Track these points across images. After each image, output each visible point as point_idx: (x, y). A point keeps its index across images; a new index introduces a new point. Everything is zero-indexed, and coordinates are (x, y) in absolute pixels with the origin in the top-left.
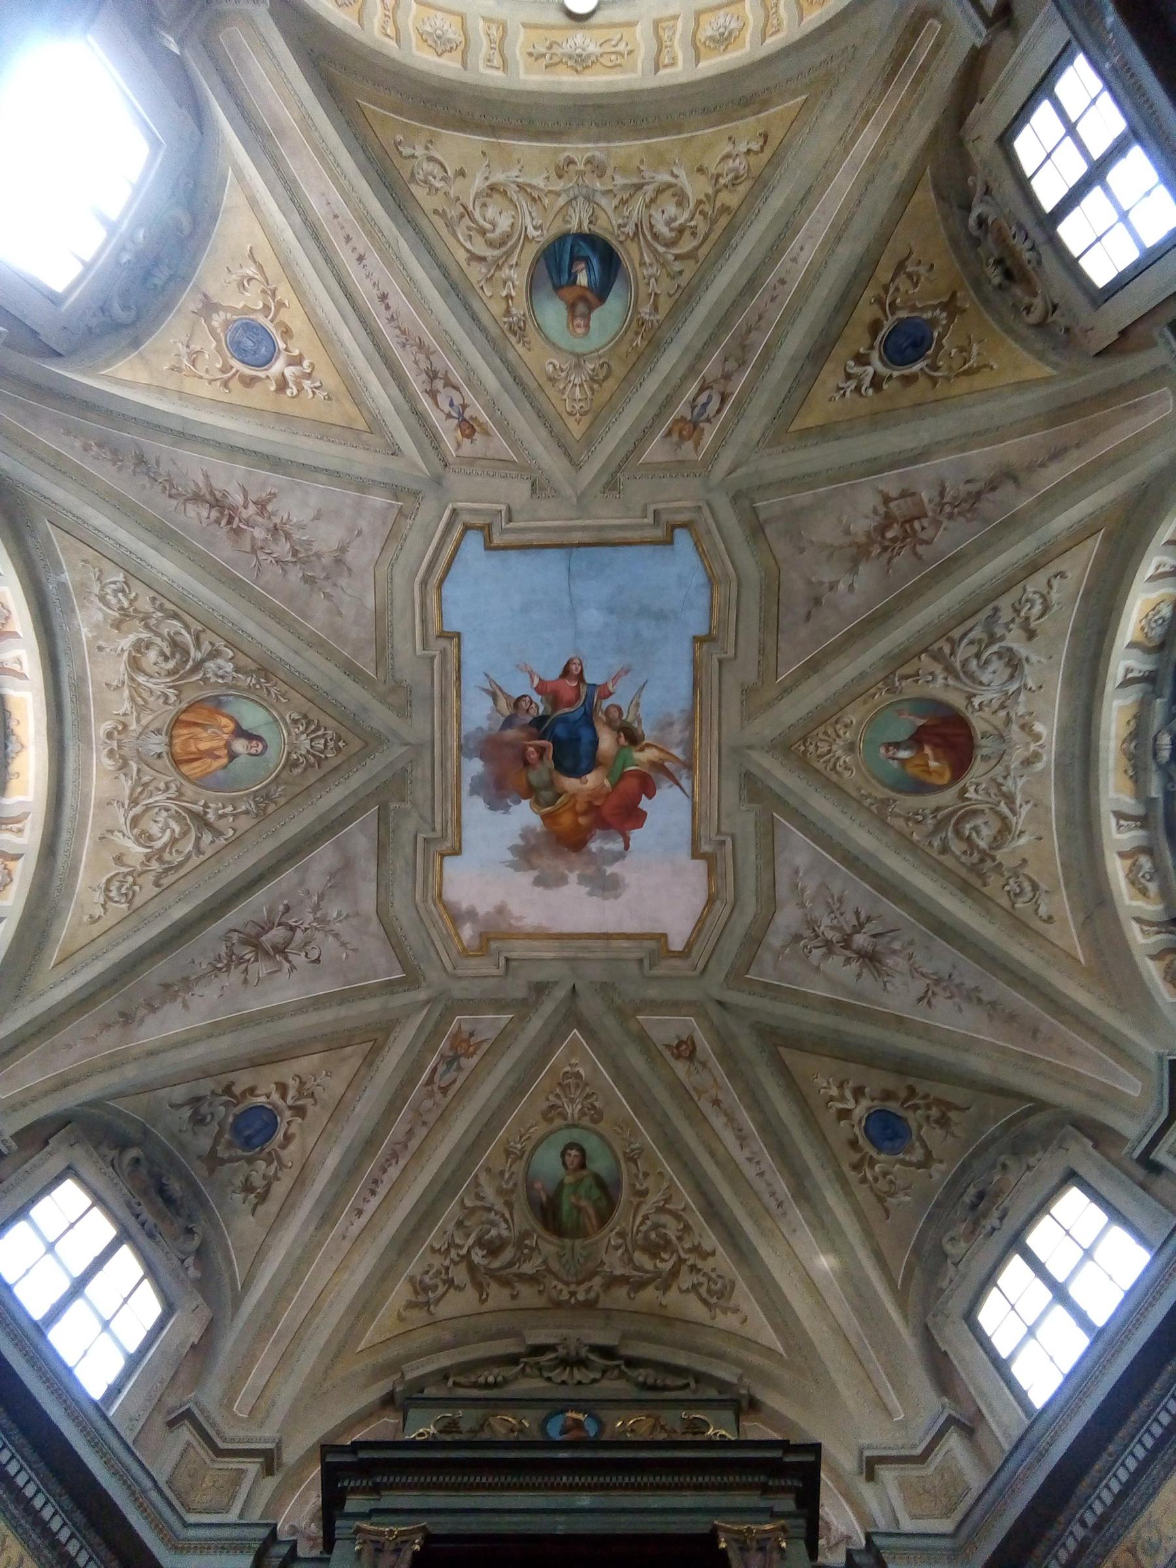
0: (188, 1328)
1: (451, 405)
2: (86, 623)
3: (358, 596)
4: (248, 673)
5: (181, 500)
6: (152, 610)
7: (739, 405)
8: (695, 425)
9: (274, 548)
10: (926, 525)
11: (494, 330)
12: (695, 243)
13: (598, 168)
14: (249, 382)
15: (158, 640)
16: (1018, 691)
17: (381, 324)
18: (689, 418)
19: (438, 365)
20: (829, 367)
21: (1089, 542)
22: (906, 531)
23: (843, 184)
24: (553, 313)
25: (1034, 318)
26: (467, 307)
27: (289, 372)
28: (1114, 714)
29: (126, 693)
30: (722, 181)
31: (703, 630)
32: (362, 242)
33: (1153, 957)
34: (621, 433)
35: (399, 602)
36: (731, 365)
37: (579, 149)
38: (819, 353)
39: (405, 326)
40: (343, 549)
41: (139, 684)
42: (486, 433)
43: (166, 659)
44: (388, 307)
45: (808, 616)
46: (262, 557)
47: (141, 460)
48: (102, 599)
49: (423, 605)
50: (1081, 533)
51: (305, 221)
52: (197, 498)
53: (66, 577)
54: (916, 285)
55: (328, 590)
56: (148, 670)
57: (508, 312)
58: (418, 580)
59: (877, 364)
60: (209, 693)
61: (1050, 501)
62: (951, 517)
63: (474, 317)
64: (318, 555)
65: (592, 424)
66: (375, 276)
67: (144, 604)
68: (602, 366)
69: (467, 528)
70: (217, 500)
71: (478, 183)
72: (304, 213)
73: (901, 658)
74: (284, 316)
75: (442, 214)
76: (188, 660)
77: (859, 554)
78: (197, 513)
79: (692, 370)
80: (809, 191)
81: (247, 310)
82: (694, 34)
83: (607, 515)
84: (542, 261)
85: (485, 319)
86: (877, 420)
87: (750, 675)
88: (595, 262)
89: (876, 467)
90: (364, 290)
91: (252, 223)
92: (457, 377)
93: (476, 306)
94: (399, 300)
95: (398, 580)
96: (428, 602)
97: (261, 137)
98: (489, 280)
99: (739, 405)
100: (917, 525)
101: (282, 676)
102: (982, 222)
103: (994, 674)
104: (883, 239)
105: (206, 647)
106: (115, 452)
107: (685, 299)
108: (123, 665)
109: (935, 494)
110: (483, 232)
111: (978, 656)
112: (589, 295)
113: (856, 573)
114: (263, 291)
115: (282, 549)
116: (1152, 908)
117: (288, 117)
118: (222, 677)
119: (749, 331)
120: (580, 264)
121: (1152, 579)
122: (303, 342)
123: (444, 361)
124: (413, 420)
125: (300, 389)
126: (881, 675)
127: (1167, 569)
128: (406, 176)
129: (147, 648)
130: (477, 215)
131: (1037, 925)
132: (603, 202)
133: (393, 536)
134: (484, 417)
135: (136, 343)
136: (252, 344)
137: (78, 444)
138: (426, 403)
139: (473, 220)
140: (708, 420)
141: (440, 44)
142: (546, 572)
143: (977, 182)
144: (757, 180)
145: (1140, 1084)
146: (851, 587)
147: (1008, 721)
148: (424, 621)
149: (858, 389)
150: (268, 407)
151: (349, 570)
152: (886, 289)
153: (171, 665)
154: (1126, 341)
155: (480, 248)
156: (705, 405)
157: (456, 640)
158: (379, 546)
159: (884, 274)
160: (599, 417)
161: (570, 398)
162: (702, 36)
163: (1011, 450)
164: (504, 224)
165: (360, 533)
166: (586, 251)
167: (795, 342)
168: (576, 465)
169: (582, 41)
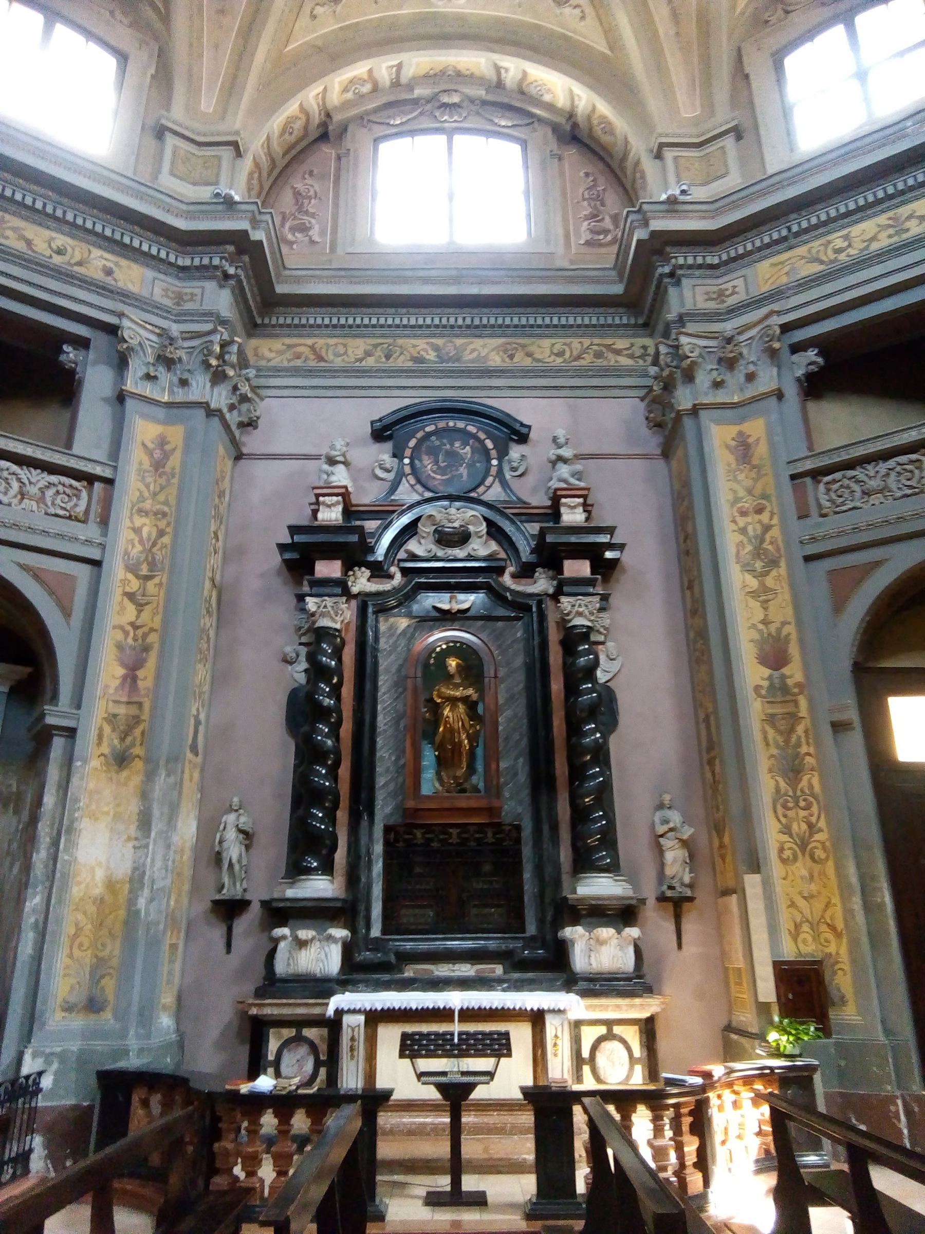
21: (604, 43)
28: (474, 59)
33: (301, 105)
50: (610, 34)
116: (335, 98)
121: (571, 92)
127: (576, 102)
131: (307, 9)
145: (211, 110)
154: (740, 76)
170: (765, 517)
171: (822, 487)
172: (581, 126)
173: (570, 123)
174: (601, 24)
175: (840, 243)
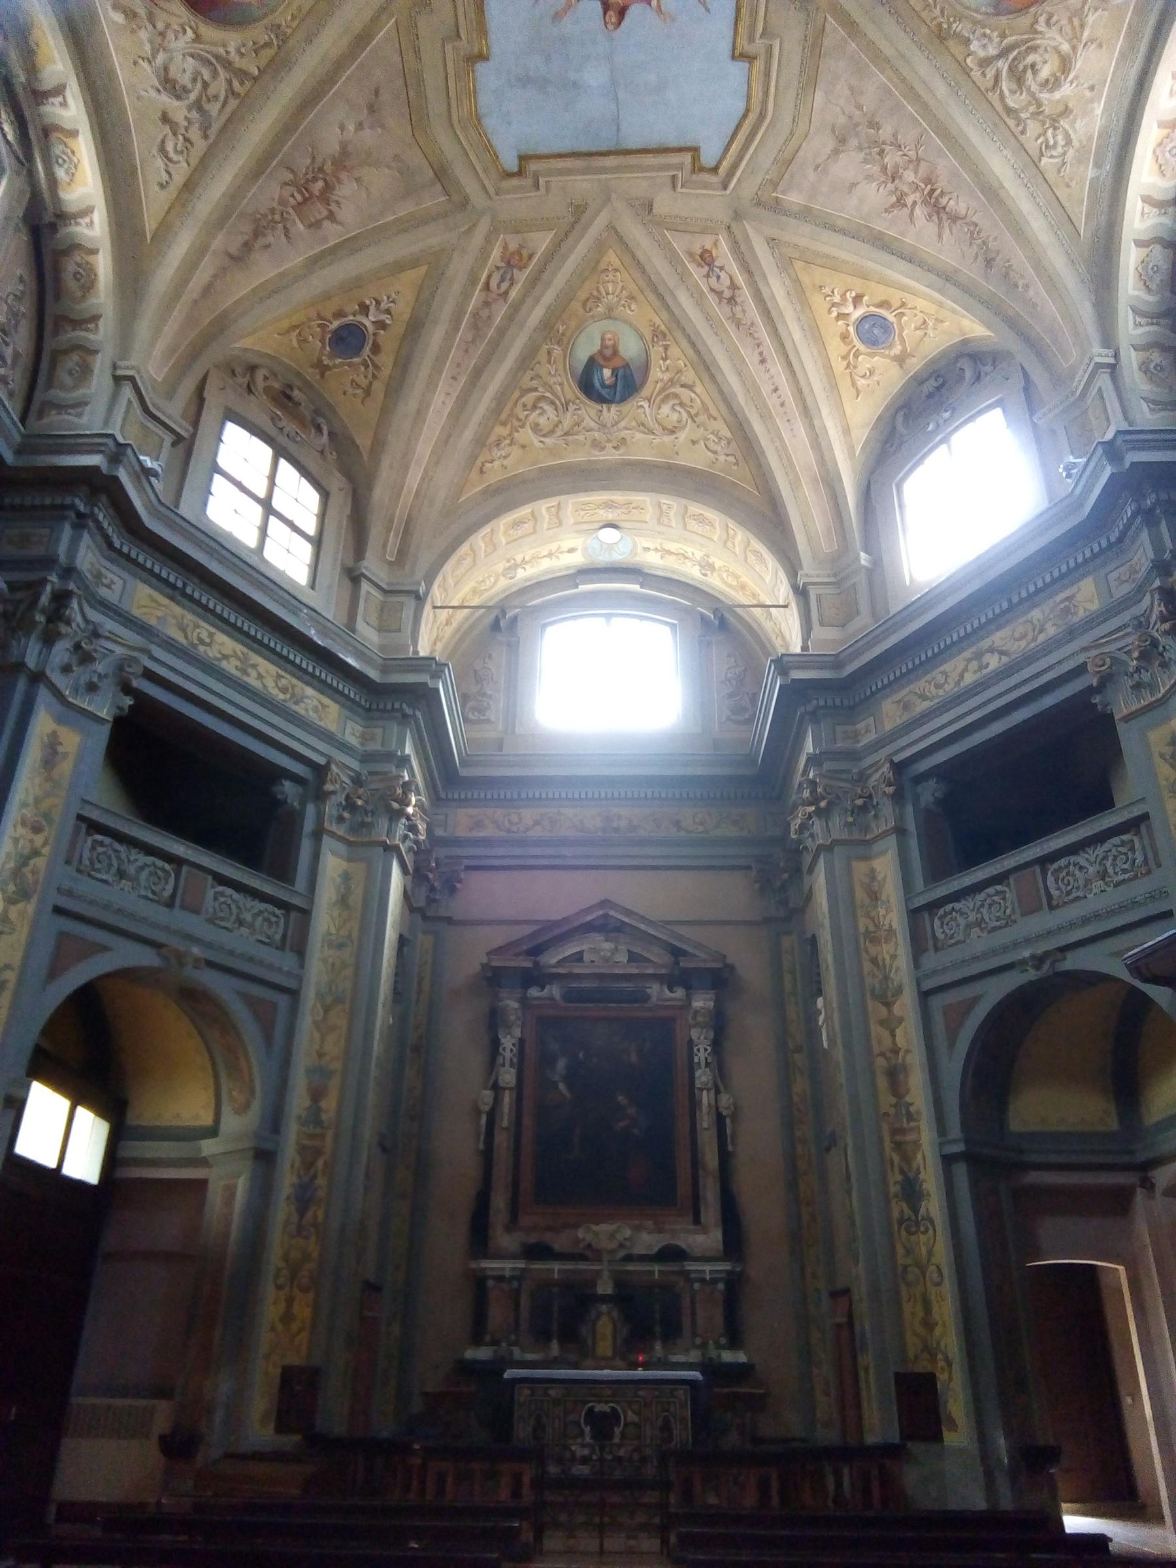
0: (341, 500)
1: (718, 277)
2: (1093, 120)
3: (830, 104)
4: (957, 35)
5: (968, 220)
6: (1029, 121)
7: (473, 281)
8: (508, 263)
9: (897, 159)
10: (291, 199)
11: (678, 334)
12: (524, 399)
13: (596, 445)
14: (884, 304)
15: (1034, 88)
16: (154, 56)
17: (767, 340)
18: (515, 271)
19: (727, 309)
20: (406, 317)
21: (154, 226)
22: (307, 190)
23: (424, 449)
24: (630, 348)
25: (260, 374)
26: (698, 352)
27: (849, 309)
29: (1086, 34)
30: (508, 441)
31: (480, 67)
32: (772, 402)
34: (572, 257)
35: (791, 94)
36: (484, 313)
37: (611, 455)
38: (415, 328)
39: (749, 339)
40: (836, 152)
41: (1070, 41)
42: (691, 254)
43: (1033, 66)
44: (761, 354)
45: (377, 93)
46: (912, 153)
47: (989, 263)
48: (1069, 142)
49: (766, 93)
50: (165, 230)
51: (811, 420)
52: (955, 218)
53: (1091, 173)
54: (353, 381)
55: (858, 112)
56: (1056, 57)
57: (666, 348)
58: (768, 120)
59: (368, 322)
60: (1004, 20)
61: (199, 252)
62: (273, 211)
63: (693, 345)
64: (860, 148)
65: (598, 262)
66: (767, 376)
67: (1033, 128)
68: (590, 310)
69: (715, 170)
70: (938, 214)
71: (682, 436)
72: (811, 426)
73: (277, 66)
74: (844, 349)
75: (710, 416)
76: (1015, 59)
77: (343, 160)
78: (959, 204)
79: (516, 308)
80: (446, 442)
81: (872, 355)
82: (535, 524)
83: (583, 185)
84: (638, 382)
85: (684, 343)
86: (358, 282)
87: (424, 25)
88: (597, 384)
89: (349, 246)
90: (777, 367)
91: (849, 420)
92: (711, 298)
93: (690, 352)
94: (750, 358)
95: (788, 119)
96: (761, 93)
97: (830, 483)
98: (679, 371)
99: (473, 281)
100: (299, 197)
101: (924, 30)
102: (319, 429)
103: (184, 69)
104: (386, 411)
105: (990, 73)
106: (1006, 275)
107: (526, 361)
108: (1078, 66)
109: (293, 231)
110: (681, 404)
111: (205, 85)
112: (601, 362)
113: (341, 142)
114: (855, 367)
115: (892, 158)
117: (807, 490)
118: (984, 35)
119: (473, 341)
120: (608, 383)
122: (832, 329)
123: (720, 311)
124: (753, 267)
125: (843, 295)
126: (291, 42)
128: (734, 444)
129: (1047, 81)
130: (685, 415)
132: (593, 424)
133: (786, 162)
134: (691, 267)
135: (965, 342)
136: (875, 331)
137: (1031, 293)
138: (740, 280)
139: (689, 413)
140: (498, 268)
141: (700, 519)
142: (644, 125)
143: (332, 457)
144: (484, 445)
146: (342, 128)
147: (151, 18)
148: (767, 75)
149: (378, 302)
150: (873, 284)
151: (833, 131)
152: (374, 376)
153: (1030, 59)
155: (685, 394)
156: (502, 280)
157: (737, 53)
158: (801, 153)
159: (378, 387)
160: (593, 267)
161: (616, 283)
162: (531, 523)
163: (244, 284)
164: (666, 409)
165: (817, 167)
166: (604, 392)
167: (436, 337)
168: (611, 228)
169: (610, 516)
170: (39, 839)
171: (90, 840)
172: (58, 235)
173: (53, 220)
174: (168, 212)
175: (204, 635)
